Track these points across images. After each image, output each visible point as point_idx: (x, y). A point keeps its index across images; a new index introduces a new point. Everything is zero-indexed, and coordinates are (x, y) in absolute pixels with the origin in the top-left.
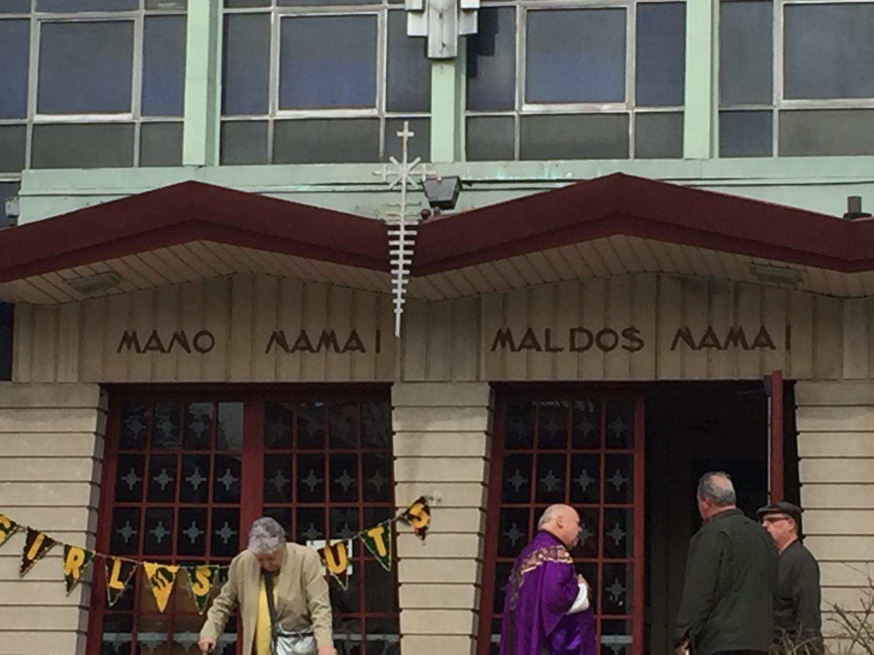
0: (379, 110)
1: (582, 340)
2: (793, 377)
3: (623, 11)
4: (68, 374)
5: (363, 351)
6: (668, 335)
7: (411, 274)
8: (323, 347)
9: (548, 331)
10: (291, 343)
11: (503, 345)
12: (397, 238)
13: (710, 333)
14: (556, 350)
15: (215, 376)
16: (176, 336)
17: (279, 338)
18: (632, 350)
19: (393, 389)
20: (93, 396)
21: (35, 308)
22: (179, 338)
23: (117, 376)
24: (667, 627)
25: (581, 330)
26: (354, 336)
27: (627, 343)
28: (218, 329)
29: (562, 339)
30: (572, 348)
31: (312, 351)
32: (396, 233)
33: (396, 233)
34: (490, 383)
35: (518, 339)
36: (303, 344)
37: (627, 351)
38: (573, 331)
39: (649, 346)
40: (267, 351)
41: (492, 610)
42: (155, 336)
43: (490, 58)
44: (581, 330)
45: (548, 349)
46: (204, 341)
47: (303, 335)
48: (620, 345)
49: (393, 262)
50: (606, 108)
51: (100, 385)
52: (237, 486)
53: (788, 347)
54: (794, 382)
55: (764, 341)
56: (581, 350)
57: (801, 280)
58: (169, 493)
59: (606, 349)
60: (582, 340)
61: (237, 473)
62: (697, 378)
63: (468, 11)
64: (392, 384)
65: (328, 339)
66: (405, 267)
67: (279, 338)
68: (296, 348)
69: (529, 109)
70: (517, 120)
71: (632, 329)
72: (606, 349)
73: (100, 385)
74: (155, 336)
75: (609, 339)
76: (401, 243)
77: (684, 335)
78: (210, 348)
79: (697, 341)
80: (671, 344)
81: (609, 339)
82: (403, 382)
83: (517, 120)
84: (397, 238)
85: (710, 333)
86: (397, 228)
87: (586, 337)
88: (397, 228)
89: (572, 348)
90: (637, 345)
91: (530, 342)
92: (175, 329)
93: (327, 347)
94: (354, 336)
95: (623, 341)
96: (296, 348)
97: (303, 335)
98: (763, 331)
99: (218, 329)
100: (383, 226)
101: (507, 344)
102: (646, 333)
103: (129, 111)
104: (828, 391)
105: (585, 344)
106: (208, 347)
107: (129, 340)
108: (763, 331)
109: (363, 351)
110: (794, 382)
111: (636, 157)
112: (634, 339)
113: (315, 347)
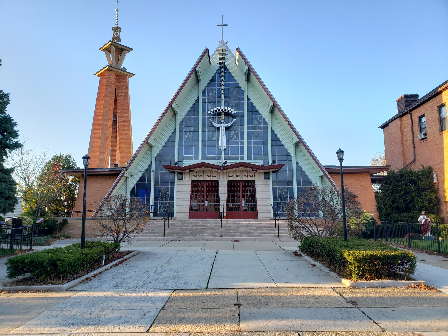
15: (202, 179)
17: (208, 176)
20: (191, 181)
21: (185, 173)
22: (199, 176)
23: (193, 179)
24: (309, 307)
28: (202, 175)
39: (242, 177)
41: (252, 222)
46: (201, 176)
52: (243, 188)
57: (390, 179)
58: (246, 187)
61: (204, 188)
65: (213, 176)
69: (230, 155)
75: (238, 176)
81: (238, 176)
92: (245, 175)
100: (220, 166)
102: (242, 176)
104: (258, 181)
107: (194, 176)
111: (268, 159)
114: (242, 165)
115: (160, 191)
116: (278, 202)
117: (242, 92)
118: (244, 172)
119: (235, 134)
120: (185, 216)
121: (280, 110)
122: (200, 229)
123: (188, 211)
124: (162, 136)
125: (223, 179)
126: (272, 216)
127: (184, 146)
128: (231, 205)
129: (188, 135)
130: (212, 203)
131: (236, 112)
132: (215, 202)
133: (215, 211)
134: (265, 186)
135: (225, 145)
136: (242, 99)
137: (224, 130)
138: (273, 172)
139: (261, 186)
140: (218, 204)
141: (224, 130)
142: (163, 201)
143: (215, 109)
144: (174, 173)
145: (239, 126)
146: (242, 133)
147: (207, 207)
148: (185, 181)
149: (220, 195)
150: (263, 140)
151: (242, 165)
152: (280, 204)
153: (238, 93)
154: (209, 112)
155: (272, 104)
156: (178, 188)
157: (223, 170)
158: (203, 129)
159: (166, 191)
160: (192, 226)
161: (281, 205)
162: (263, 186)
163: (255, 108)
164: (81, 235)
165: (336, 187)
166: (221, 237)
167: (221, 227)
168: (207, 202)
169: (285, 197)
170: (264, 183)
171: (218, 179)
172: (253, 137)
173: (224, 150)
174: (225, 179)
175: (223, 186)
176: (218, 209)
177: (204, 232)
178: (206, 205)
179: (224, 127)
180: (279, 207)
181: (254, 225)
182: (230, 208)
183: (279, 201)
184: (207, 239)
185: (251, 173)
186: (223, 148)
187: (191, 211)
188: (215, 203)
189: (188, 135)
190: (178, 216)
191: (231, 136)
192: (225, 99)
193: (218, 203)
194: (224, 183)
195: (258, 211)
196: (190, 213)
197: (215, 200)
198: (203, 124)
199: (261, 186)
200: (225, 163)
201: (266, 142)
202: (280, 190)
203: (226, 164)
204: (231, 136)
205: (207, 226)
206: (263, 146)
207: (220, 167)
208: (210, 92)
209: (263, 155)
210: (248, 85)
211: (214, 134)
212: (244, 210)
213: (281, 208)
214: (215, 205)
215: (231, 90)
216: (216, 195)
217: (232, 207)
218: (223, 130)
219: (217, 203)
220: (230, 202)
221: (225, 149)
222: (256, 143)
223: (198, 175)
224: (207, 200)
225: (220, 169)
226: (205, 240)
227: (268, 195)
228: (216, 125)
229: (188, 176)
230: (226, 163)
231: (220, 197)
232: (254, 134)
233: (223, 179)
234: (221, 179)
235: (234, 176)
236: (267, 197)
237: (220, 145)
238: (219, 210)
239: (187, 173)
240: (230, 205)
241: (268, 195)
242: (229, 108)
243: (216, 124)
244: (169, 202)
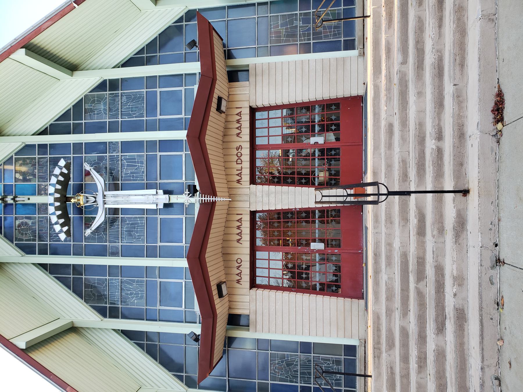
0: (183, 217)
1: (239, 161)
2: (249, 106)
3: (161, 156)
4: (247, 299)
5: (242, 218)
6: (238, 139)
7: (217, 196)
8: (240, 123)
9: (237, 170)
10: (239, 131)
11: (240, 121)
12: (205, 200)
13: (237, 128)
14: (242, 168)
16: (237, 269)
17: (238, 241)
18: (242, 148)
19: (252, 210)
22: (238, 268)
23: (248, 285)
25: (237, 161)
26: (238, 221)
27: (240, 149)
28: (236, 257)
29: (239, 166)
30: (241, 164)
31: (242, 232)
32: (203, 200)
33: (203, 200)
34: (250, 185)
35: (239, 178)
36: (240, 234)
37: (242, 149)
38: (237, 164)
40: (242, 244)
42: (237, 275)
43: (174, 192)
44: (237, 161)
45: (241, 170)
46: (239, 261)
47: (238, 234)
48: (240, 151)
49: (211, 201)
50: (184, 159)
51: (250, 290)
53: (241, 108)
54: (250, 106)
55: (239, 114)
56: (242, 161)
59: (242, 155)
60: (239, 161)
62: (249, 131)
63: (157, 193)
64: (250, 211)
66: (213, 197)
67: (238, 241)
68: (240, 130)
70: (186, 182)
71: (237, 148)
72: (242, 155)
73: (250, 290)
74: (237, 275)
76: (206, 199)
77: (238, 135)
78: (241, 153)
79: (240, 238)
80: (240, 138)
81: (239, 154)
82: (250, 208)
83: (186, 182)
84: (205, 200)
85: (237, 128)
86: (202, 200)
87: (238, 160)
88: (202, 200)
89: (241, 164)
90: (240, 147)
91: (239, 175)
92: (236, 136)
93: (241, 181)
94: (238, 221)
95: (239, 150)
96: (240, 130)
97: (238, 234)
98: (237, 114)
99: (236, 257)
101: (240, 180)
102: (238, 145)
103: (182, 283)
104: (253, 98)
105: (240, 160)
106: (240, 260)
108: (237, 114)
109: (242, 218)
110: (250, 106)
112: (239, 148)
113: (241, 231)
114: (199, 138)
115: (281, 380)
116: (312, 42)
117: (28, 148)
118: (227, 139)
119: (128, 166)
120: (355, 312)
121: (38, 30)
122: (421, 285)
123: (341, 299)
124: (130, 365)
125: (246, 198)
126: (353, 53)
127: (158, 307)
128: (322, 176)
129: (131, 294)
130: (317, 231)
131: (62, 163)
132: (314, 222)
133: (338, 222)
134: (266, 77)
135: (153, 191)
136: (43, 147)
137: (115, 196)
138: (229, 55)
139: (266, 90)
140: (320, 211)
141: (115, 196)
142: (310, 374)
143: (54, 219)
144: (230, 341)
145: (108, 154)
146: (127, 146)
147: (327, 245)
148: (253, 308)
149: (292, 207)
150: (145, 90)
151: (199, 138)
152: (317, 35)
153: (28, 161)
154: (63, 236)
155: (21, 54)
156: (273, 328)
157: (215, 194)
158: (114, 254)
159: (282, 362)
160: (405, 312)
161: (320, 33)
162: (266, 82)
163: (65, 116)
164: (337, 195)
165: (318, 114)
166: (466, 192)
167: (409, 193)
168: (312, 244)
169: (299, 23)
170: (259, 78)
171: (249, 213)
172: (136, 117)
173: (167, 196)
174: (247, 191)
175: (265, 199)
176: (334, 213)
177: (439, 270)
178: (321, 246)
179: (104, 196)
180: (326, 37)
181: (396, 67)
182: (331, 179)
183: (309, 40)
184: (169, 188)
185: (230, 119)
186: (163, 199)
187: (340, 290)
188: (317, 221)
189: (131, 294)
190: (355, 332)
191: (133, 177)
192: (43, 192)
193: (317, 211)
194: (259, 194)
195: (340, 95)
196: (344, 296)
197: (307, 222)
198: (102, 252)
199: (266, 90)
200: (193, 190)
201: (151, 81)
202: (280, 37)
203: (198, 188)
204: (133, 177)
205: (405, 257)
206: (158, 90)
207: (203, 205)
208: (26, 234)
209: (182, 89)
210: (14, 134)
211: (128, 224)
212: (337, 139)
213: (334, 31)
214: (322, 222)
215: (21, 178)
216: (292, 218)
217: (327, 174)
218: (113, 199)
219: (317, 216)
220: (314, 179)
221: (166, 192)
222: (151, 110)
223: (235, 269)
224: (308, 245)
225: (213, 204)
226: (492, 272)
227: (292, 68)
228: (100, 219)
229: (237, 298)
230: (195, 186)
231: (299, 206)
232: (129, 115)
233: (246, 198)
234: (247, 205)
235: (239, 166)
236: (299, 71)
237: (154, 207)
238: (335, 209)
239: (230, 301)
240: (322, 179)
241: (292, 68)
242: (54, 180)
243: (98, 217)
244: (312, 355)
